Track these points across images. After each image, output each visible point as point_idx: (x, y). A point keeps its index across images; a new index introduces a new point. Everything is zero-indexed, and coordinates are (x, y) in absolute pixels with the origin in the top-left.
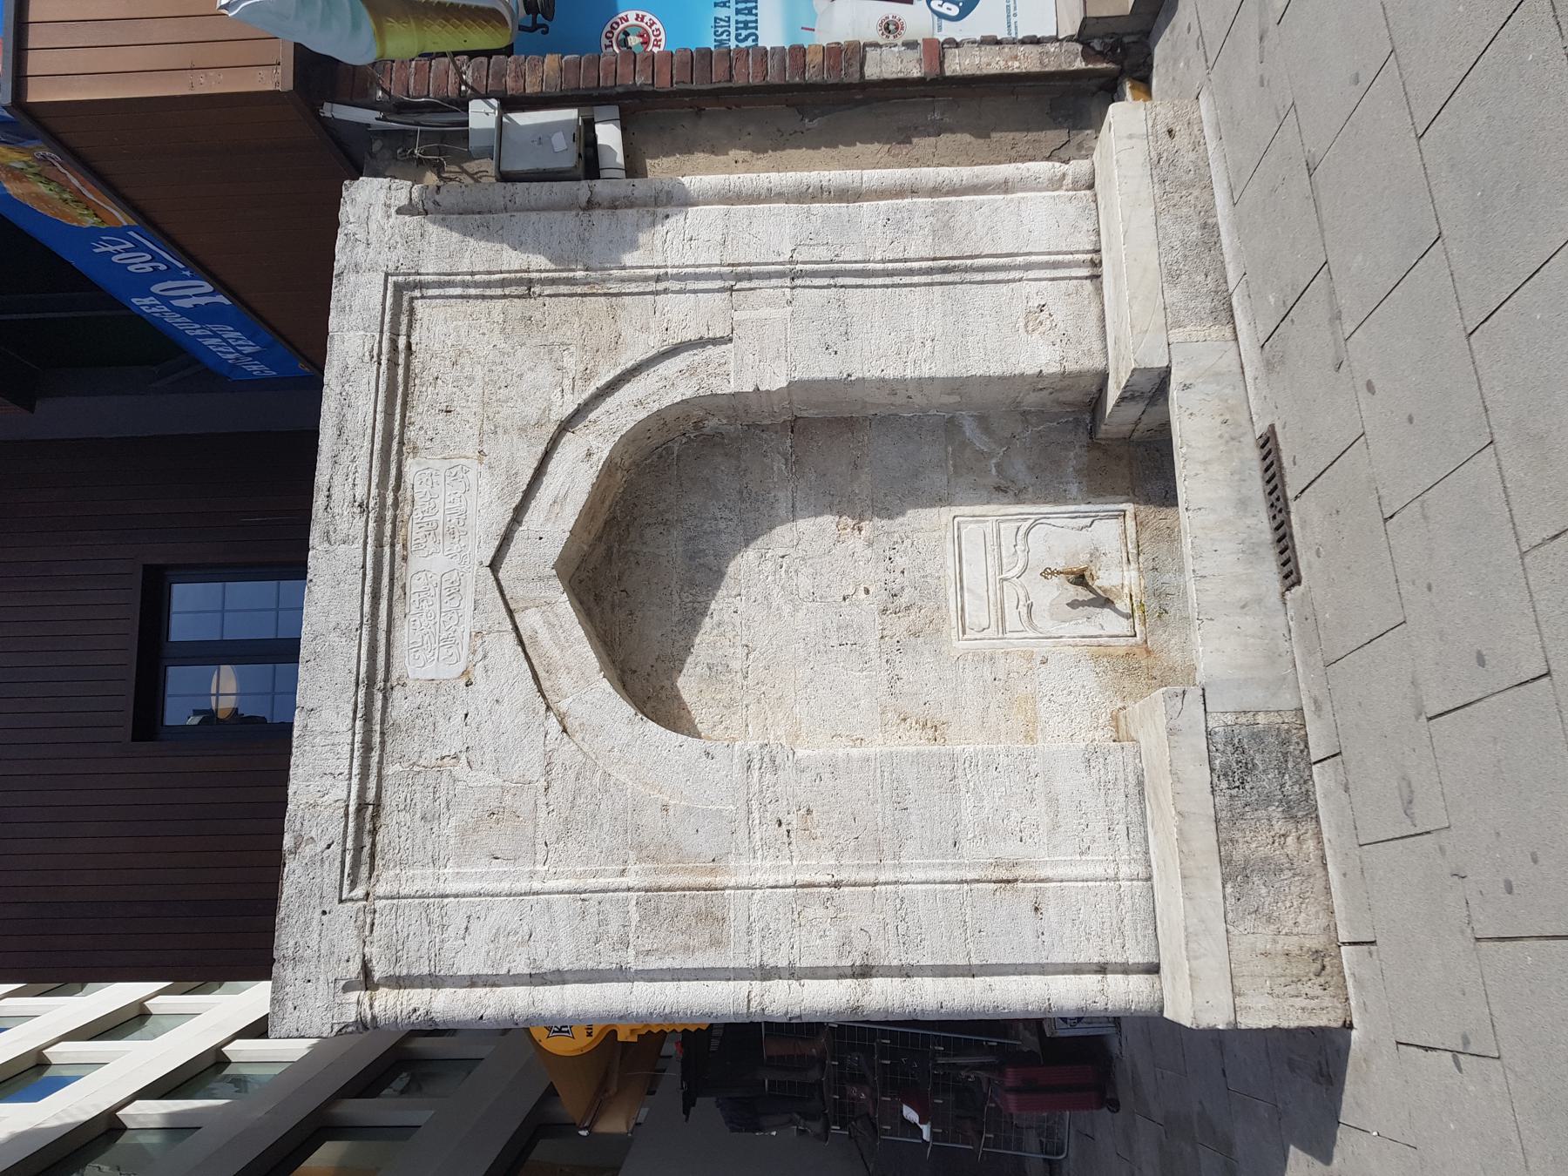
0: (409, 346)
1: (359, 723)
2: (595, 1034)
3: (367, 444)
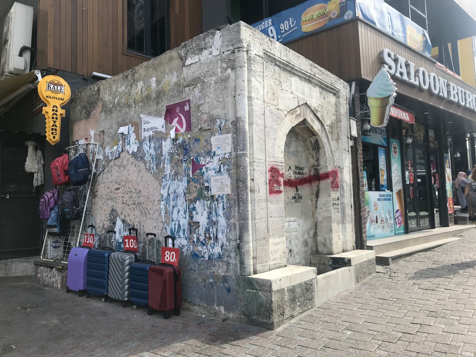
2: (47, 99)
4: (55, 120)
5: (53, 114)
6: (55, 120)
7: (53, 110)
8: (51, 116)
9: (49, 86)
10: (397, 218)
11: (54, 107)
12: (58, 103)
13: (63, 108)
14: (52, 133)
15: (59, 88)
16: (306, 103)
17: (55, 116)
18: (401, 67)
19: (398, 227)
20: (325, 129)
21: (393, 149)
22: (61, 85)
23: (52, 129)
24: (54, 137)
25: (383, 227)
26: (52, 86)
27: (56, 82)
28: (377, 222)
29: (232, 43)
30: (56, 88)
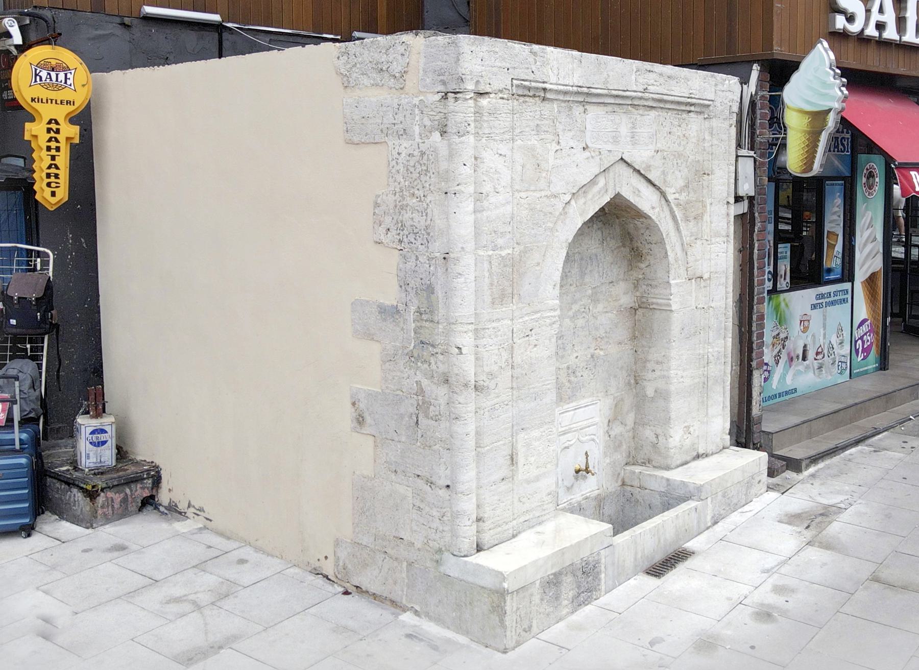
0: (690, 112)
1: (575, 89)
2: (33, 104)
3: (665, 92)
4: (53, 152)
5: (50, 140)
6: (53, 152)
7: (49, 130)
8: (44, 145)
9: (36, 75)
10: (861, 338)
11: (50, 122)
12: (61, 113)
13: (73, 120)
14: (49, 185)
15: (62, 76)
16: (622, 159)
17: (53, 144)
18: (881, 10)
19: (860, 359)
20: (667, 201)
21: (864, 180)
22: (66, 69)
23: (48, 176)
24: (53, 194)
25: (820, 368)
26: (44, 74)
27: (54, 62)
28: (804, 359)
29: (442, 77)
30: (54, 78)
